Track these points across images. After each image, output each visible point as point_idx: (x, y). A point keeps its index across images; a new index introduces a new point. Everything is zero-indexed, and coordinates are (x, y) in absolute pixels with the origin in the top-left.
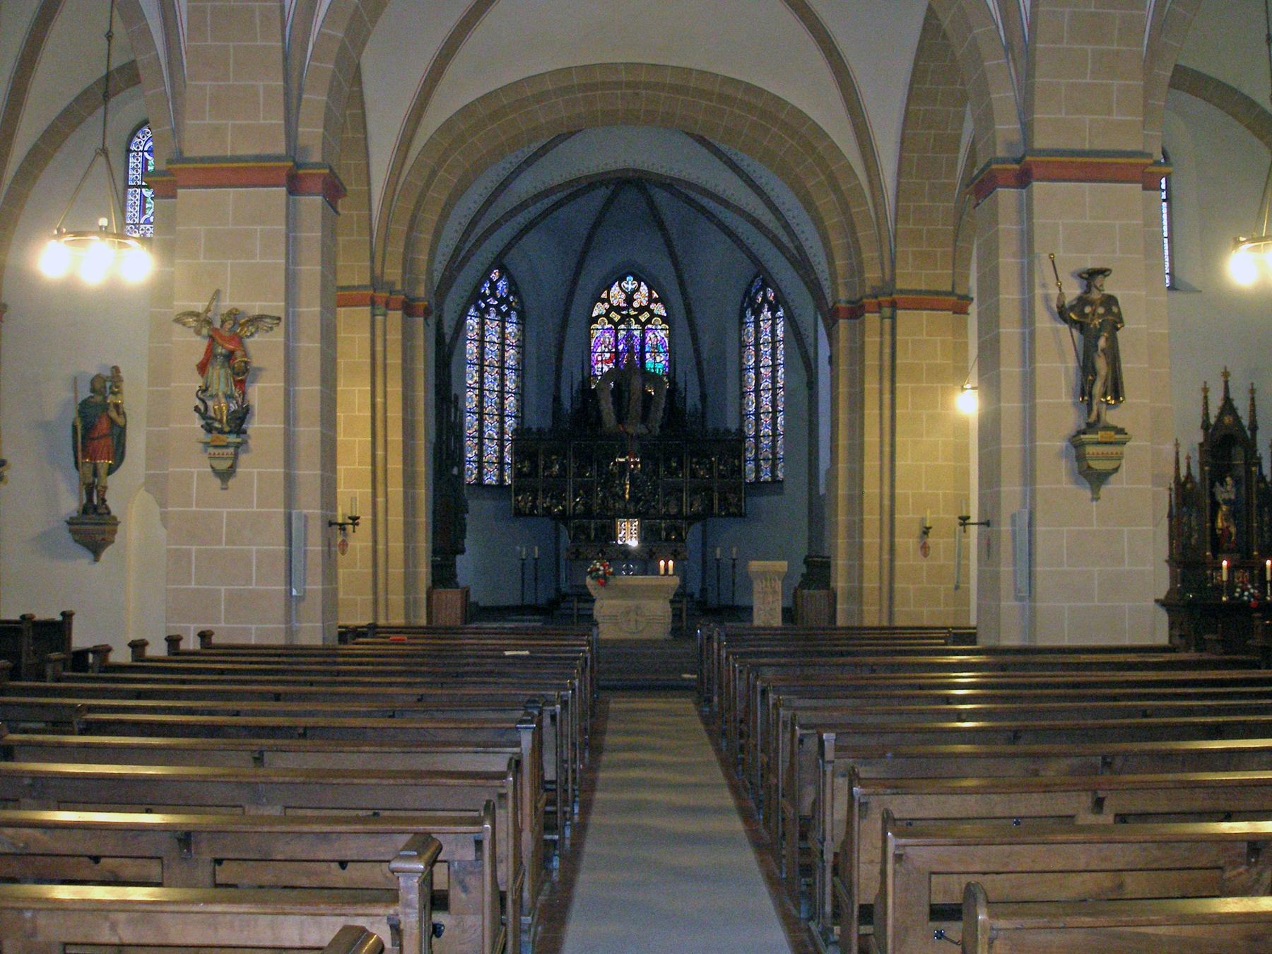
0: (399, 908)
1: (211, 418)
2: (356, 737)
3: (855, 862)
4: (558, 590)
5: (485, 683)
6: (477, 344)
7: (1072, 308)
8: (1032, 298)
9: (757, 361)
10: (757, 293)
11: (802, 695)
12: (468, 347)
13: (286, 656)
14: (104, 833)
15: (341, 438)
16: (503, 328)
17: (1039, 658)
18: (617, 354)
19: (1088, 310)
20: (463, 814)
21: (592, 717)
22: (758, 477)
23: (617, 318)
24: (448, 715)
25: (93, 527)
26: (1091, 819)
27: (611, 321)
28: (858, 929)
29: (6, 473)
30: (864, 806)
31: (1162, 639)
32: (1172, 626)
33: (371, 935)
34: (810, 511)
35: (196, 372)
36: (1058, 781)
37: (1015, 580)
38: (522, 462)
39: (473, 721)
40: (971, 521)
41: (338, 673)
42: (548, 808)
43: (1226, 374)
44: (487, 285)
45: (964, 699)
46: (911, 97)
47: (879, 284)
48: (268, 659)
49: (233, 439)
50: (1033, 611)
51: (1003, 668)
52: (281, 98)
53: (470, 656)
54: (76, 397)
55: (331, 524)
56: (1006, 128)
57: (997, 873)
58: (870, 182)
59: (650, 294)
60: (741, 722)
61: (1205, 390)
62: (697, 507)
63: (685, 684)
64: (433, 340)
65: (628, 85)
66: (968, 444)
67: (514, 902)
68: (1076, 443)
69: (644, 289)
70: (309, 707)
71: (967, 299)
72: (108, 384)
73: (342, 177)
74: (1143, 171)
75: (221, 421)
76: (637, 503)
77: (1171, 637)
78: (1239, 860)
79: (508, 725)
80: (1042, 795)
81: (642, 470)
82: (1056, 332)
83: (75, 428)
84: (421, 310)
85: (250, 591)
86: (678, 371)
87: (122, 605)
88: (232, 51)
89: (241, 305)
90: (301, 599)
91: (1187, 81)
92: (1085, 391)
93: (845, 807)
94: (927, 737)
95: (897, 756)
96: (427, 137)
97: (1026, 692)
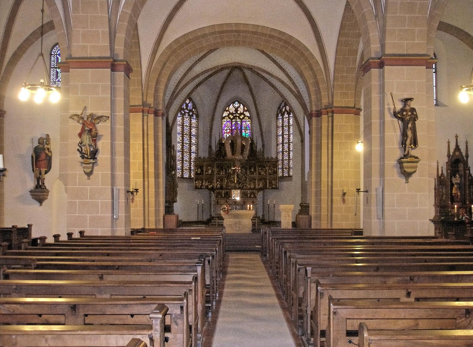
0: (152, 332)
1: (84, 153)
2: (138, 269)
3: (319, 314)
4: (211, 215)
5: (184, 249)
6: (181, 126)
7: (399, 113)
8: (384, 109)
9: (283, 133)
10: (282, 108)
11: (299, 253)
12: (178, 127)
13: (112, 240)
14: (43, 306)
15: (131, 160)
16: (191, 121)
17: (386, 240)
18: (232, 130)
19: (405, 113)
20: (176, 297)
21: (223, 261)
22: (283, 175)
23: (232, 117)
24: (171, 261)
25: (39, 193)
26: (406, 300)
27: (230, 118)
28: (320, 340)
29: (6, 174)
30: (322, 294)
31: (432, 234)
32: (436, 229)
33: (142, 342)
34: (302, 187)
35: (78, 136)
36: (393, 285)
37: (377, 212)
38: (197, 169)
39: (180, 263)
40: (361, 190)
41: (131, 246)
42: (207, 295)
43: (457, 137)
44: (185, 105)
45: (358, 255)
46: (340, 35)
47: (328, 104)
48: (105, 241)
49: (92, 161)
50: (384, 223)
51: (373, 244)
52: (108, 35)
53: (178, 240)
54: (33, 145)
55: (128, 192)
56: (375, 47)
57: (371, 319)
58: (324, 67)
59: (244, 109)
60: (277, 263)
61: (449, 142)
62: (261, 185)
63: (257, 249)
64: (165, 125)
65: (236, 31)
66: (360, 163)
67: (195, 329)
68: (400, 162)
69: (242, 106)
70: (120, 258)
71: (360, 109)
72: (45, 141)
73: (131, 65)
74: (427, 62)
75: (87, 154)
76: (239, 184)
77: (435, 233)
78: (462, 316)
79: (192, 264)
80: (387, 291)
81: (241, 172)
82: (393, 121)
83: (32, 157)
84: (161, 114)
85: (98, 216)
86: (254, 136)
87: (50, 222)
88: (89, 18)
89: (94, 112)
90: (117, 219)
91: (445, 27)
92: (403, 143)
93: (315, 294)
94: (345, 269)
95: (334, 276)
96: (162, 50)
97: (381, 253)
